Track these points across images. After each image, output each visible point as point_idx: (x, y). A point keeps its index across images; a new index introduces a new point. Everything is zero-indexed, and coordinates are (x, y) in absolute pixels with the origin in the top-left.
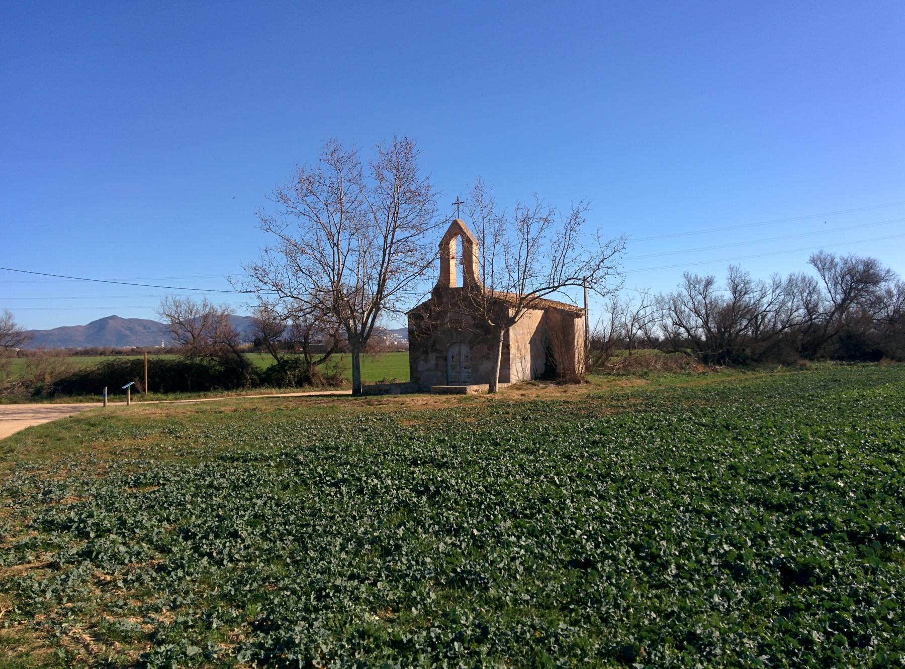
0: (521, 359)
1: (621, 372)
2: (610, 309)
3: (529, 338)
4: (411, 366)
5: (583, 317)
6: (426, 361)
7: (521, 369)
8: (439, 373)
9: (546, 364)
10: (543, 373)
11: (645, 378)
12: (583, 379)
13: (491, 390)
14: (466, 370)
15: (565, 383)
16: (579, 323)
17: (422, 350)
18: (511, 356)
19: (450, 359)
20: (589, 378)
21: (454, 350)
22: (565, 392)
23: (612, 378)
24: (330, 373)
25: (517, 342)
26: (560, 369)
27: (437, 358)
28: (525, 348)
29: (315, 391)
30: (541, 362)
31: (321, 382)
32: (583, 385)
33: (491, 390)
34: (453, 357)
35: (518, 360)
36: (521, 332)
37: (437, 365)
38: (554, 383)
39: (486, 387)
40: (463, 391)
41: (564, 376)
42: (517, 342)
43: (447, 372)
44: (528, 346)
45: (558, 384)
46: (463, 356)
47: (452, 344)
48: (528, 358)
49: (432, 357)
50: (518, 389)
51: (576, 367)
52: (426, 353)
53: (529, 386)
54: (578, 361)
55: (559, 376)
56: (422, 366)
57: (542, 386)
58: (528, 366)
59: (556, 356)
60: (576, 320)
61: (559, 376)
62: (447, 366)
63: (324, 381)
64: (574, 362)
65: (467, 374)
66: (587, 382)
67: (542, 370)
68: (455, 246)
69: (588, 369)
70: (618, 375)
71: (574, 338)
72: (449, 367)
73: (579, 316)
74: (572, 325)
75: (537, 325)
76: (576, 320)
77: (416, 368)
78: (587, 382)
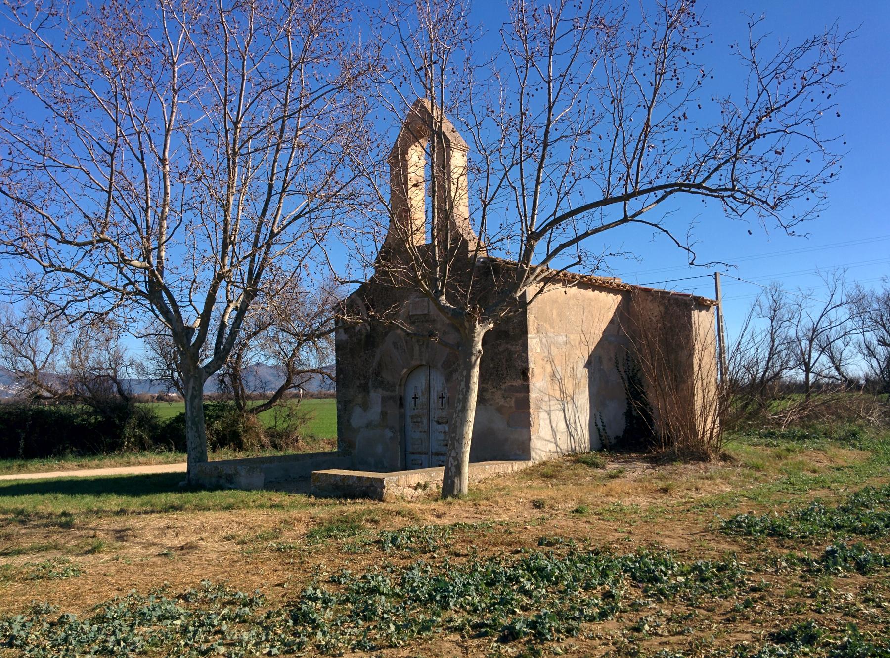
0: (563, 401)
1: (798, 430)
2: (766, 310)
3: (583, 354)
4: (339, 417)
5: (713, 309)
6: (365, 406)
7: (562, 426)
8: (389, 434)
9: (629, 415)
10: (621, 434)
11: (854, 446)
12: (716, 449)
13: (449, 490)
14: (440, 428)
15: (671, 459)
16: (702, 321)
17: (358, 383)
18: (533, 395)
19: (409, 401)
20: (731, 447)
21: (419, 382)
22: (665, 490)
23: (784, 445)
24: (281, 426)
25: (552, 362)
26: (659, 428)
27: (384, 400)
28: (574, 377)
29: (129, 464)
30: (616, 411)
31: (259, 440)
32: (715, 466)
33: (449, 490)
34: (415, 398)
35: (555, 406)
36: (562, 339)
37: (384, 414)
38: (645, 460)
39: (435, 476)
40: (373, 491)
41: (671, 444)
42: (552, 362)
43: (403, 430)
44: (583, 373)
45: (656, 461)
46: (434, 396)
47: (413, 370)
48: (583, 400)
49: (376, 396)
50: (546, 477)
51: (699, 421)
52: (365, 389)
53: (581, 470)
54: (704, 407)
55: (657, 441)
56: (358, 419)
57: (612, 467)
58: (583, 418)
59: (651, 396)
60: (695, 314)
61: (657, 441)
62: (403, 417)
63: (265, 440)
64: (692, 411)
65: (442, 437)
66: (725, 458)
67: (618, 427)
68: (416, 157)
69: (727, 425)
70: (792, 437)
71: (691, 355)
72: (409, 420)
73: (701, 304)
74: (687, 326)
75: (604, 326)
76: (695, 314)
77: (348, 421)
78: (725, 458)
